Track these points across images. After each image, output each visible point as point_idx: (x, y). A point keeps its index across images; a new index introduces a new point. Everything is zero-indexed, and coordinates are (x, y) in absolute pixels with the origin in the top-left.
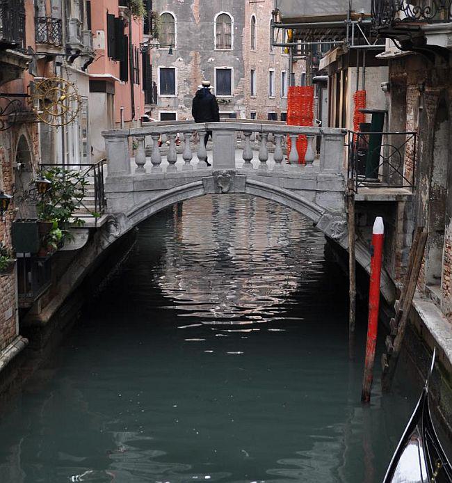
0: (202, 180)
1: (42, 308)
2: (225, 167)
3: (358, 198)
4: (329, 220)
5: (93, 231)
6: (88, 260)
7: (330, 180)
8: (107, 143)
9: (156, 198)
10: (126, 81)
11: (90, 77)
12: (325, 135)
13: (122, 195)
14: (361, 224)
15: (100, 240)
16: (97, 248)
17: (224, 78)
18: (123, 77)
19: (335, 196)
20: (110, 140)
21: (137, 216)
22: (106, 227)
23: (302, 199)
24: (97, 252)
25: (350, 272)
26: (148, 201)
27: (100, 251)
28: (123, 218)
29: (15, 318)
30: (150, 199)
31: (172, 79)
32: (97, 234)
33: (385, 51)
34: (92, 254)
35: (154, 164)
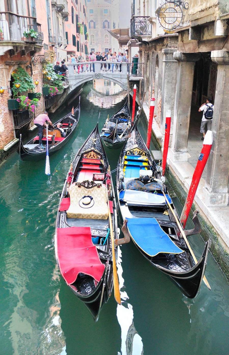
1: (53, 109)
3: (130, 80)
5: (65, 89)
6: (65, 97)
7: (124, 75)
10: (79, 51)
18: (78, 50)
19: (125, 79)
22: (68, 88)
27: (67, 94)
33: (78, 15)
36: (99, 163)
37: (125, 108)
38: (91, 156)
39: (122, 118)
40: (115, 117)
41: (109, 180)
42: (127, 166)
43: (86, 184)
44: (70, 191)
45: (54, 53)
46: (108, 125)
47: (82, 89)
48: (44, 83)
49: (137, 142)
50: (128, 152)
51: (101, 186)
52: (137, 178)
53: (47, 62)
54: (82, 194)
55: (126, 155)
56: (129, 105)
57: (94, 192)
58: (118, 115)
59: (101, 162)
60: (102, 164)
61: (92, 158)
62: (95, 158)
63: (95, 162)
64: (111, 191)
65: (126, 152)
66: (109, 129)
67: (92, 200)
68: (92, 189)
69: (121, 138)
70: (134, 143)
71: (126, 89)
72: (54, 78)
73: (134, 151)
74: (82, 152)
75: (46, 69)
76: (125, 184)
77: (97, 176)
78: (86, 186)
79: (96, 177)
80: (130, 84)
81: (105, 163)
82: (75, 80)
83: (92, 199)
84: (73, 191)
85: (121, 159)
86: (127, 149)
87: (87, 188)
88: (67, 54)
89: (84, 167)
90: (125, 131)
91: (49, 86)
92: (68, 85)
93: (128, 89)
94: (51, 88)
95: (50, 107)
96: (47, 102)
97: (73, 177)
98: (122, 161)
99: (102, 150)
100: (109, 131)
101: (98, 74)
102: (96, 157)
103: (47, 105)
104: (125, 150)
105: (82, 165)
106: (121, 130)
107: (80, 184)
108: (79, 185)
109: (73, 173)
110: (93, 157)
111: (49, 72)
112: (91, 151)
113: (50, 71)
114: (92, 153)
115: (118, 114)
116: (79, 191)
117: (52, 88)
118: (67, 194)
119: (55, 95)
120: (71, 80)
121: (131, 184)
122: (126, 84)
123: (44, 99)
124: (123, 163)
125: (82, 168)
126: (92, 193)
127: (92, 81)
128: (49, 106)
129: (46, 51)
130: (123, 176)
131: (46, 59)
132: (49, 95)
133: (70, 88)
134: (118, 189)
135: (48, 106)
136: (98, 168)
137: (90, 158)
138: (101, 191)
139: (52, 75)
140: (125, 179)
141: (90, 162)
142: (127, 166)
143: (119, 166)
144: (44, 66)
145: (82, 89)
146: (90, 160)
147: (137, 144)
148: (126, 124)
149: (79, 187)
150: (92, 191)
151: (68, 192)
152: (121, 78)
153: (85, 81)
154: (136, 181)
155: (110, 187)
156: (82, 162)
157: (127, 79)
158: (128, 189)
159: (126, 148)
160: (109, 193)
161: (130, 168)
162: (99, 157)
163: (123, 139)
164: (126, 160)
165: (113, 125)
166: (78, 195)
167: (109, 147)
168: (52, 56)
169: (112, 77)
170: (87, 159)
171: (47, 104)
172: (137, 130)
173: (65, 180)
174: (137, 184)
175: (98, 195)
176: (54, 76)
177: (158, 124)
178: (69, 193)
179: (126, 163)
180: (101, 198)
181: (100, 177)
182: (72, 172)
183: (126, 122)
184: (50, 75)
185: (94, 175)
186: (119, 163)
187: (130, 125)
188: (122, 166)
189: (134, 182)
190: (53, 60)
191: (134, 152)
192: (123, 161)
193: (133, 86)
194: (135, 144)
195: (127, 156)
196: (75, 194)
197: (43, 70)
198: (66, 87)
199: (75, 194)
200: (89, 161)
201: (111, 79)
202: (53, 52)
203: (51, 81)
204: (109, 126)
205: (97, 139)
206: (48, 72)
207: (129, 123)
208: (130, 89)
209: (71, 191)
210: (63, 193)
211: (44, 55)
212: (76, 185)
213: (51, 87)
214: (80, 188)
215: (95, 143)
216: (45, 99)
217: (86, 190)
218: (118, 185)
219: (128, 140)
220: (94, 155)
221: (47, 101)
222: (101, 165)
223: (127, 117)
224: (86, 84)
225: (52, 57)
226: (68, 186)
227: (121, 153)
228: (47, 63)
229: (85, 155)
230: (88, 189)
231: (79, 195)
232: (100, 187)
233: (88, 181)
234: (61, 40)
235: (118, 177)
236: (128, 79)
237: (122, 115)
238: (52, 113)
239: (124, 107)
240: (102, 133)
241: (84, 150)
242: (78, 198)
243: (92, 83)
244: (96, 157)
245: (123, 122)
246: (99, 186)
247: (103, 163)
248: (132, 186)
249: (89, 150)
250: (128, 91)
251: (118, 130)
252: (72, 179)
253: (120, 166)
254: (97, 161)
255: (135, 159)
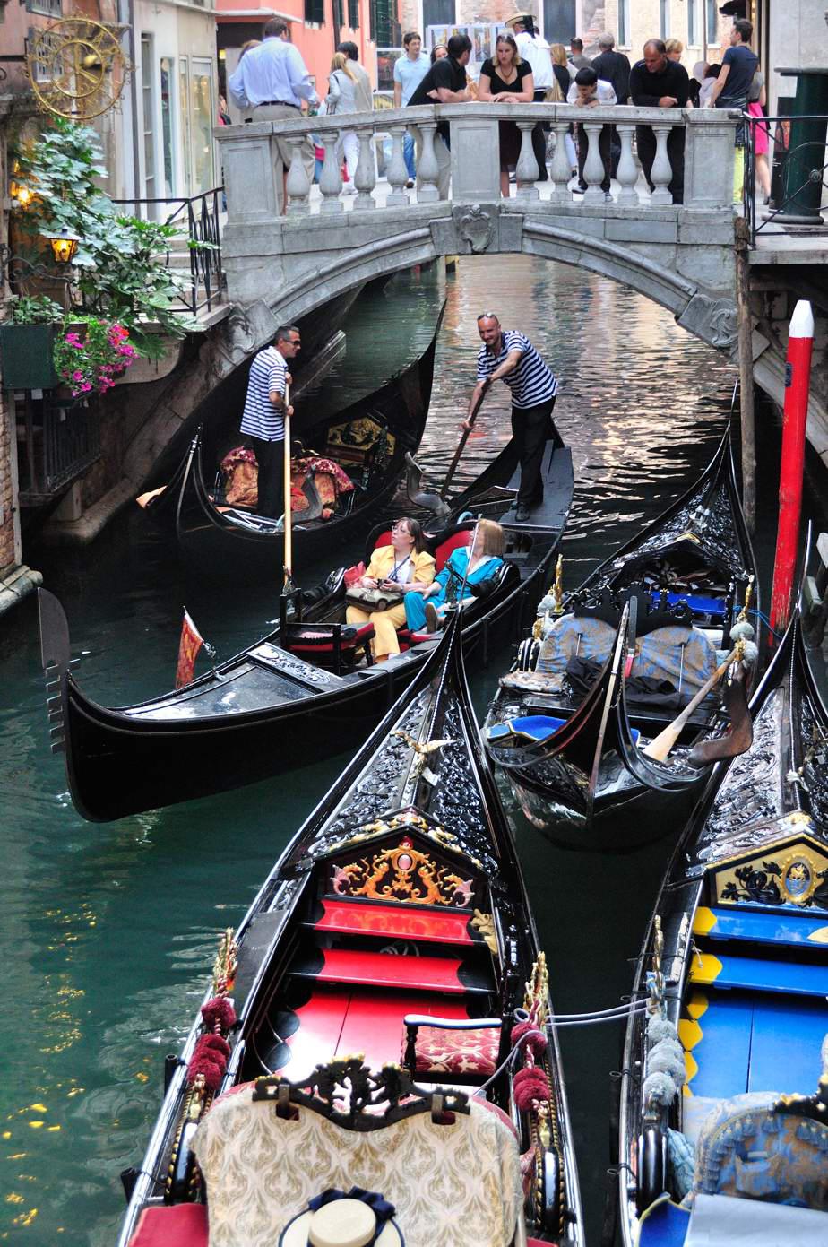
0: (429, 226)
1: (85, 507)
2: (478, 197)
3: (757, 259)
5: (194, 342)
7: (706, 220)
8: (225, 151)
9: (332, 266)
10: (320, 20)
11: (218, 17)
12: (694, 124)
13: (260, 262)
15: (213, 361)
16: (207, 377)
17: (561, 11)
19: (717, 255)
20: (232, 146)
21: (290, 308)
23: (647, 263)
24: (208, 384)
26: (314, 274)
27: (214, 382)
28: (260, 310)
30: (317, 268)
31: (450, 12)
32: (206, 346)
34: (195, 389)
35: (326, 194)
36: (463, 938)
37: (705, 504)
38: (390, 876)
41: (533, 1075)
42: (717, 995)
43: (338, 1090)
44: (208, 1145)
46: (551, 648)
47: (341, 334)
48: (14, 290)
49: (803, 795)
50: (725, 879)
51: (467, 1111)
52: (799, 1097)
53: (47, 115)
54: (302, 1175)
55: (708, 901)
56: (748, 479)
58: (648, 565)
59: (473, 931)
60: (486, 947)
61: (401, 894)
62: (424, 893)
63: (429, 930)
64: (550, 1157)
65: (710, 878)
66: (560, 677)
67: (389, 1229)
68: (390, 1132)
69: (663, 759)
71: (722, 342)
72: (99, 245)
73: (774, 868)
74: (322, 846)
75: (40, 175)
76: (686, 1146)
77: (440, 1043)
78: (343, 1107)
79: (432, 1049)
80: (760, 294)
81: (506, 932)
82: (278, 263)
83: (385, 1214)
84: (233, 1149)
85: (660, 937)
86: (719, 850)
88: (220, 47)
89: (331, 972)
90: (699, 696)
91: (56, 312)
92: (219, 301)
93: (740, 335)
94: (72, 328)
95: (66, 490)
96: (38, 445)
98: (668, 957)
99: (486, 832)
100: (560, 696)
101: (477, 214)
102: (432, 887)
104: (701, 854)
105: (319, 961)
106: (667, 687)
107: (294, 1089)
108: (284, 1097)
109: (239, 1007)
110: (407, 887)
111: (57, 192)
112: (393, 839)
113: (67, 184)
114: (405, 856)
115: (645, 548)
116: (279, 1152)
118: (181, 1175)
119: (109, 389)
120: (251, 264)
121: (741, 1146)
123: (12, 420)
124: (678, 968)
126: (388, 1170)
127: (426, 266)
128: (49, 481)
129: (42, 25)
130: (680, 1081)
131: (36, 90)
132: (56, 392)
133: (239, 332)
134: (632, 1195)
136: (450, 982)
137: (385, 896)
138: (462, 1151)
139: (89, 220)
140: (691, 1103)
141: (382, 931)
142: (717, 995)
143: (644, 992)
144: (23, 148)
145: (341, 334)
146: (382, 916)
147: (807, 809)
148: (717, 635)
149: (285, 1112)
150: (392, 1147)
151: (192, 1159)
152: (679, 245)
153: (366, 273)
154: (791, 1123)
155: (545, 1134)
156: (318, 925)
157: (729, 254)
159: (707, 844)
160: (529, 1175)
161: (745, 1014)
162: (464, 887)
163: (678, 763)
164: (706, 944)
165: (599, 642)
166: (271, 1179)
167: (558, 831)
168: (90, 59)
170: (365, 903)
171: (38, 462)
172: (803, 688)
173: (172, 1066)
175: (435, 1184)
176: (99, 228)
178: (203, 1161)
179: (710, 970)
180: (459, 1210)
181: (465, 1051)
182: (231, 1001)
183: (715, 623)
184: (70, 220)
185: (413, 1029)
186: (649, 966)
187: (751, 649)
188: (669, 997)
189: (774, 1135)
190: (100, 95)
191: (778, 880)
192: (683, 952)
193: (789, 317)
194: (788, 809)
195: (716, 907)
197: (12, 177)
198: (198, 322)
199: (245, 1171)
200: (376, 923)
202: (97, 30)
203: (77, 272)
204: (564, 651)
205: (449, 741)
206: (55, 200)
207: (740, 627)
208: (759, 344)
209: (218, 1146)
211: (20, 58)
212: (260, 1096)
213: (77, 320)
214: (291, 1123)
215: (433, 778)
216: (19, 421)
217: (341, 1145)
218: (627, 1155)
219: (729, 775)
221: (38, 437)
222: (474, 958)
223: (723, 578)
224: (376, 293)
225: (86, 75)
226: (194, 1108)
227: (666, 884)
228: (45, 123)
229: (343, 874)
230: (357, 1138)
231: (283, 1185)
232: (451, 1121)
233: (354, 1069)
234: (118, 236)
235: (637, 1081)
236: (744, 254)
237: (683, 557)
239: (697, 490)
240: (498, 708)
241: (340, 832)
242: (271, 1205)
243: (431, 292)
244: (432, 887)
245: (686, 624)
246: (446, 1107)
247: (493, 941)
248: (751, 1168)
249: (382, 828)
251: (640, 684)
252: (228, 1055)
253: (655, 989)
254: (443, 922)
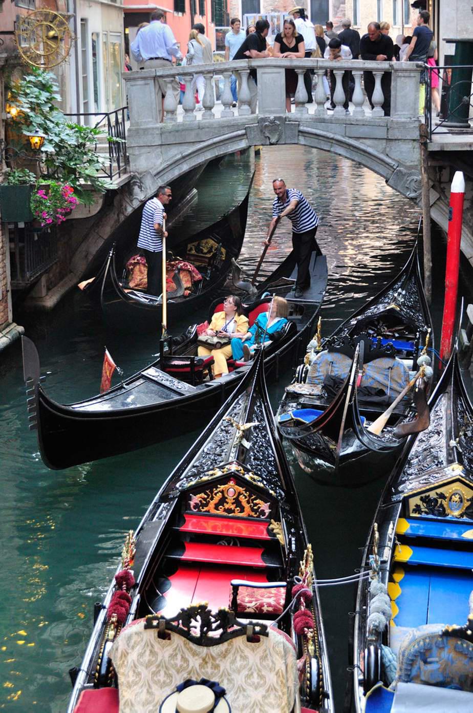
0: (245, 129)
1: (49, 289)
3: (432, 148)
4: (404, 175)
5: (111, 194)
8: (129, 86)
9: (190, 151)
10: (183, 11)
12: (396, 71)
13: (148, 149)
14: (442, 180)
15: (122, 205)
16: (118, 215)
17: (320, 5)
20: (133, 83)
23: (370, 150)
24: (119, 219)
25: (102, 298)
26: (179, 156)
27: (122, 218)
28: (149, 177)
29: (6, 302)
30: (181, 153)
35: (186, 110)
36: (265, 536)
37: (403, 288)
38: (223, 500)
39: (386, 337)
40: (356, 330)
41: (305, 614)
42: (410, 569)
43: (193, 623)
45: (62, 23)
46: (315, 370)
47: (195, 191)
48: (8, 165)
49: (459, 454)
50: (414, 502)
51: (267, 635)
52: (456, 627)
54: (172, 671)
55: (405, 515)
56: (427, 274)
57: (233, 662)
58: (370, 322)
59: (270, 532)
60: (278, 541)
61: (229, 511)
62: (242, 510)
63: (245, 531)
65: (405, 501)
66: (320, 387)
67: (222, 702)
68: (225, 645)
69: (379, 433)
70: (443, 456)
71: (413, 195)
72: (57, 139)
73: (442, 496)
74: (184, 484)
75: (23, 100)
76: (392, 655)
77: (252, 596)
78: (196, 632)
79: (247, 599)
80: (434, 168)
81: (289, 532)
82: (159, 150)
83: (220, 694)
84: (133, 656)
85: (377, 535)
86: (411, 485)
87: (197, 641)
88: (126, 26)
89: (189, 555)
91: (32, 178)
92: (125, 171)
93: (423, 191)
95: (38, 280)
96: (21, 254)
97: (137, 598)
98: (381, 547)
99: (278, 475)
100: (320, 397)
101: (272, 122)
102: (247, 507)
103: (23, 271)
104: (400, 488)
105: (183, 549)
106: (381, 393)
108: (163, 627)
109: (136, 575)
110: (233, 507)
111: (33, 109)
112: (224, 479)
113: (38, 105)
114: (231, 489)
115: (369, 313)
116: (160, 658)
117: (47, 187)
118: (103, 671)
119: (62, 222)
120: (144, 150)
121: (423, 654)
122: (411, 167)
123: (7, 240)
124: (387, 553)
125: (180, 560)
126: (222, 668)
127: (243, 152)
128: (28, 274)
129: (24, 13)
130: (388, 617)
131: (21, 51)
132: (32, 223)
134: (361, 683)
135: (23, 276)
136: (256, 560)
137: (220, 512)
138: (264, 658)
139: (51, 125)
140: (395, 630)
141: (218, 532)
142: (410, 569)
143: (368, 566)
144: (13, 84)
145: (195, 191)
146: (219, 523)
147: (461, 462)
148: (410, 362)
149: (163, 635)
150: (224, 655)
151: (110, 662)
152: (388, 140)
153: (209, 156)
154: (452, 642)
155: (311, 648)
156: (182, 528)
157: (417, 145)
158: (409, 678)
159: (404, 482)
160: (302, 671)
161: (424, 580)
162: (265, 507)
163: (387, 436)
164: (403, 539)
165: (342, 366)
166: (155, 674)
167: (319, 474)
168: (52, 33)
169: (345, 136)
171: (22, 263)
172: (459, 393)
173: (98, 609)
174: (453, 655)
175: (249, 676)
176: (57, 130)
177: (161, 128)
178: (116, 663)
179: (406, 554)
180: (262, 691)
181: (266, 600)
182: (132, 572)
184: (40, 125)
185: (236, 588)
186: (371, 552)
187: (429, 370)
188: (382, 570)
190: (57, 54)
191: (444, 503)
192: (390, 544)
193: (451, 181)
194: (450, 462)
195: (409, 518)
196: (140, 669)
197: (7, 101)
198: (113, 184)
199: (140, 669)
200: (215, 527)
201: (339, 142)
202: (56, 16)
204: (322, 372)
205: (257, 423)
207: (423, 358)
208: (434, 196)
209: (125, 654)
210: (85, 666)
212: (148, 626)
213: (44, 183)
215: (247, 445)
216: (11, 240)
217: (195, 654)
218: (358, 660)
219: (417, 443)
220: (242, 498)
221: (21, 249)
222: (271, 547)
223: (413, 330)
224: (214, 165)
225: (49, 42)
226: (111, 633)
227: (380, 505)
228: (26, 70)
229: (196, 499)
230: (204, 650)
231: (162, 677)
232: (258, 640)
233: (202, 611)
235: (362, 627)
236: (425, 145)
237: (390, 318)
238: (43, 311)
239: (398, 280)
240: (285, 405)
241: (195, 475)
242: (155, 688)
244: (247, 507)
245: (392, 356)
246: (255, 633)
247: (281, 537)
248: (430, 667)
249: (218, 473)
250: (422, 203)
251: (366, 391)
253: (374, 565)
254: (254, 527)
255: (452, 534)
